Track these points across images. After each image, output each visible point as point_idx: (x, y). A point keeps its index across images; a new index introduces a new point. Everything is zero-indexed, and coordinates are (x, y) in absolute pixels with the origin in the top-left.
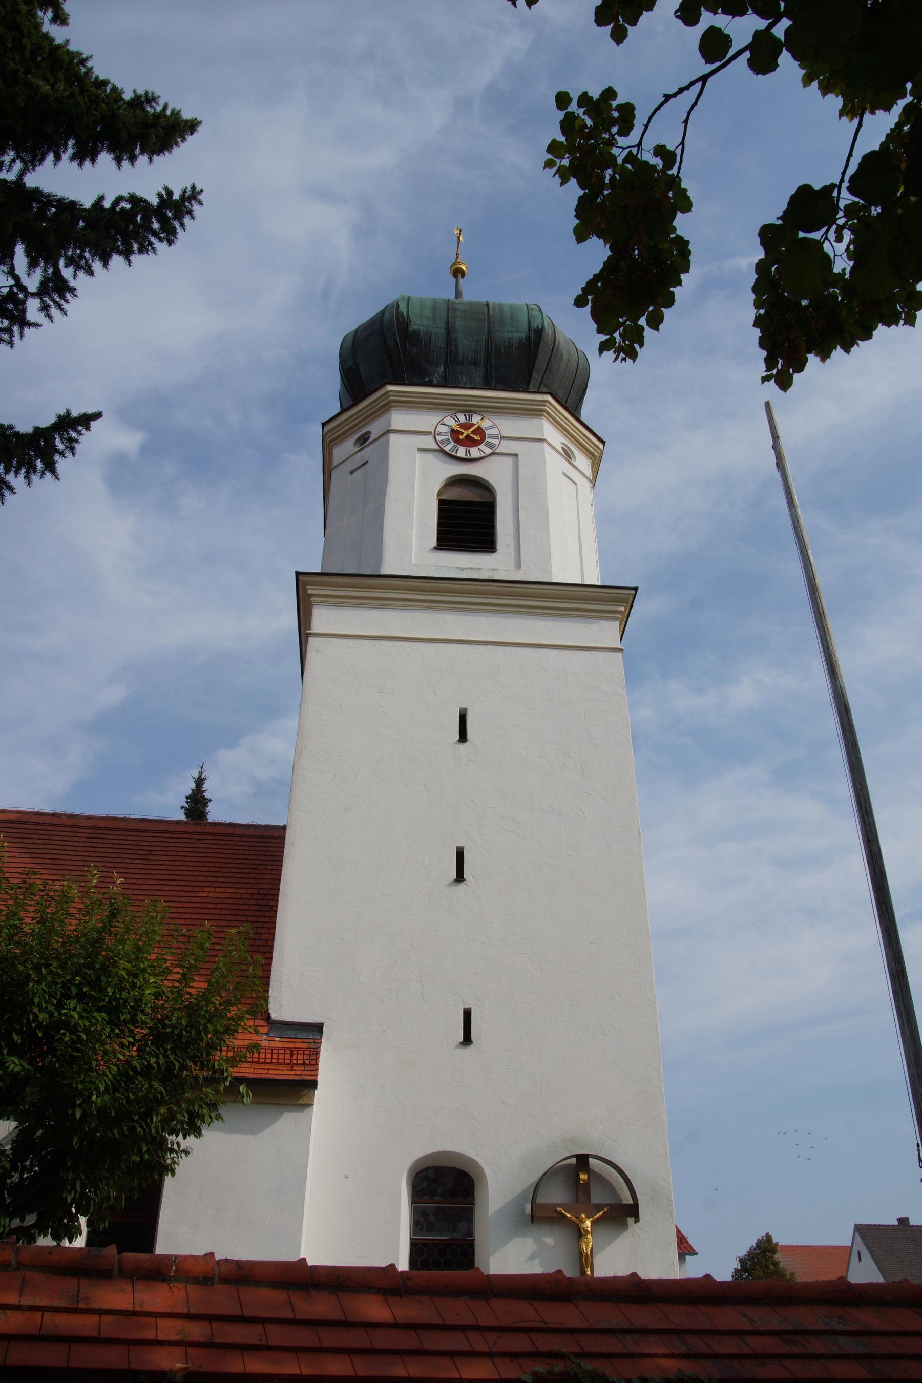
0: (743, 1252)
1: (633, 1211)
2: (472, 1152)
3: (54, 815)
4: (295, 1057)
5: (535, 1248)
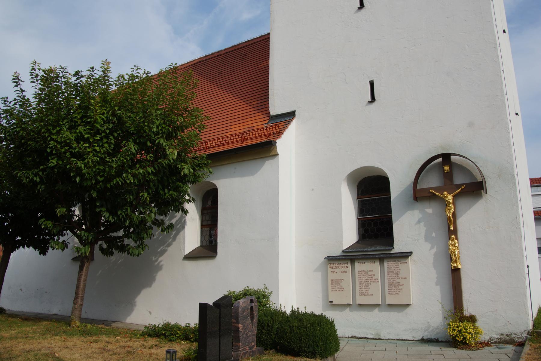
3: (206, 56)
4: (268, 130)
5: (421, 216)
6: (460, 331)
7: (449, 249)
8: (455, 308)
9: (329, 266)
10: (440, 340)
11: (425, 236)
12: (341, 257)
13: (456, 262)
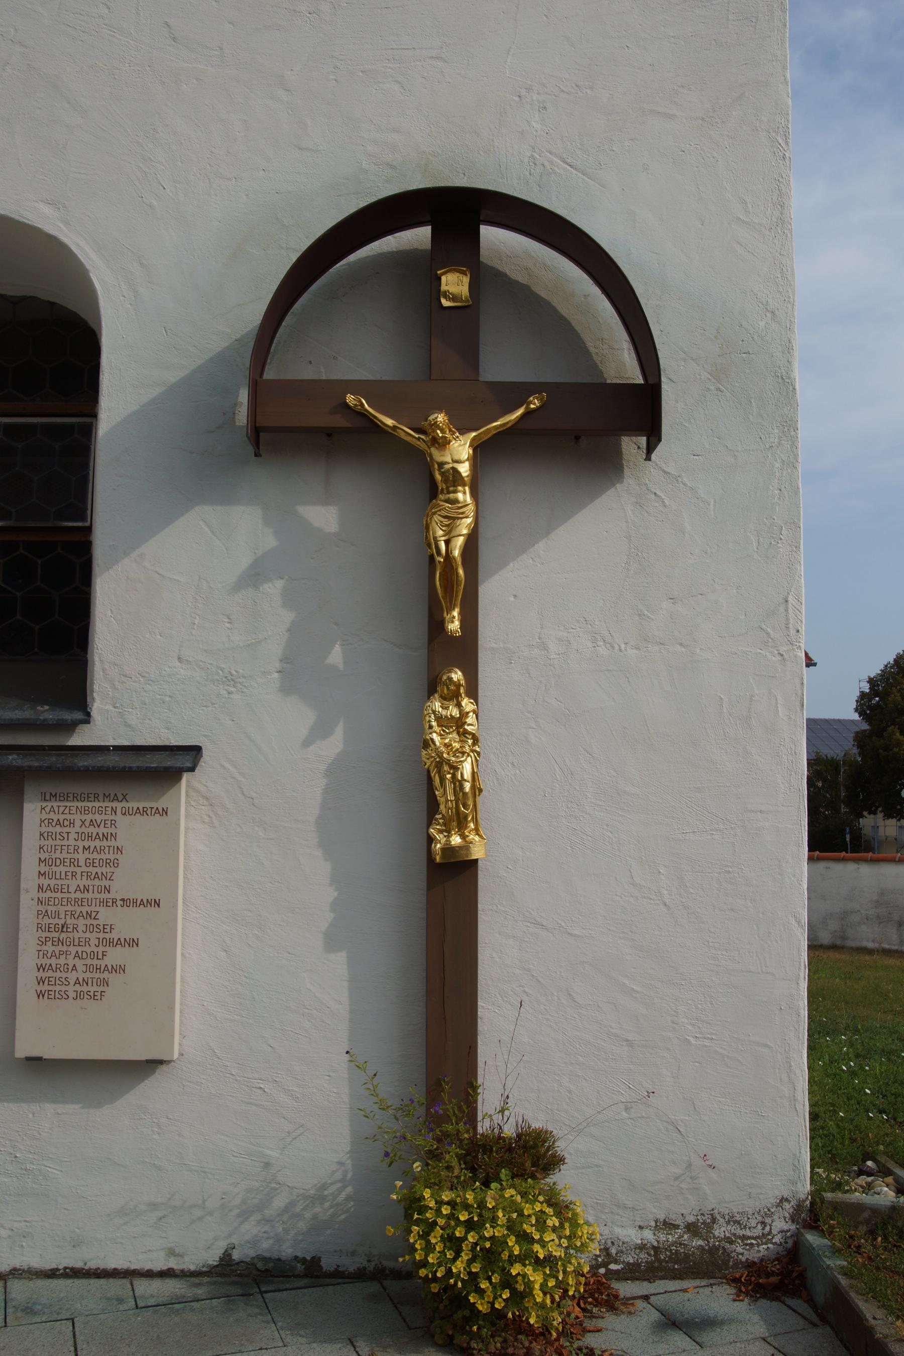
0: (875, 670)
1: (640, 410)
2: (46, 210)
5: (269, 541)
6: (490, 1256)
7: (427, 744)
8: (434, 1089)
10: (328, 1264)
11: (285, 659)
13: (460, 822)
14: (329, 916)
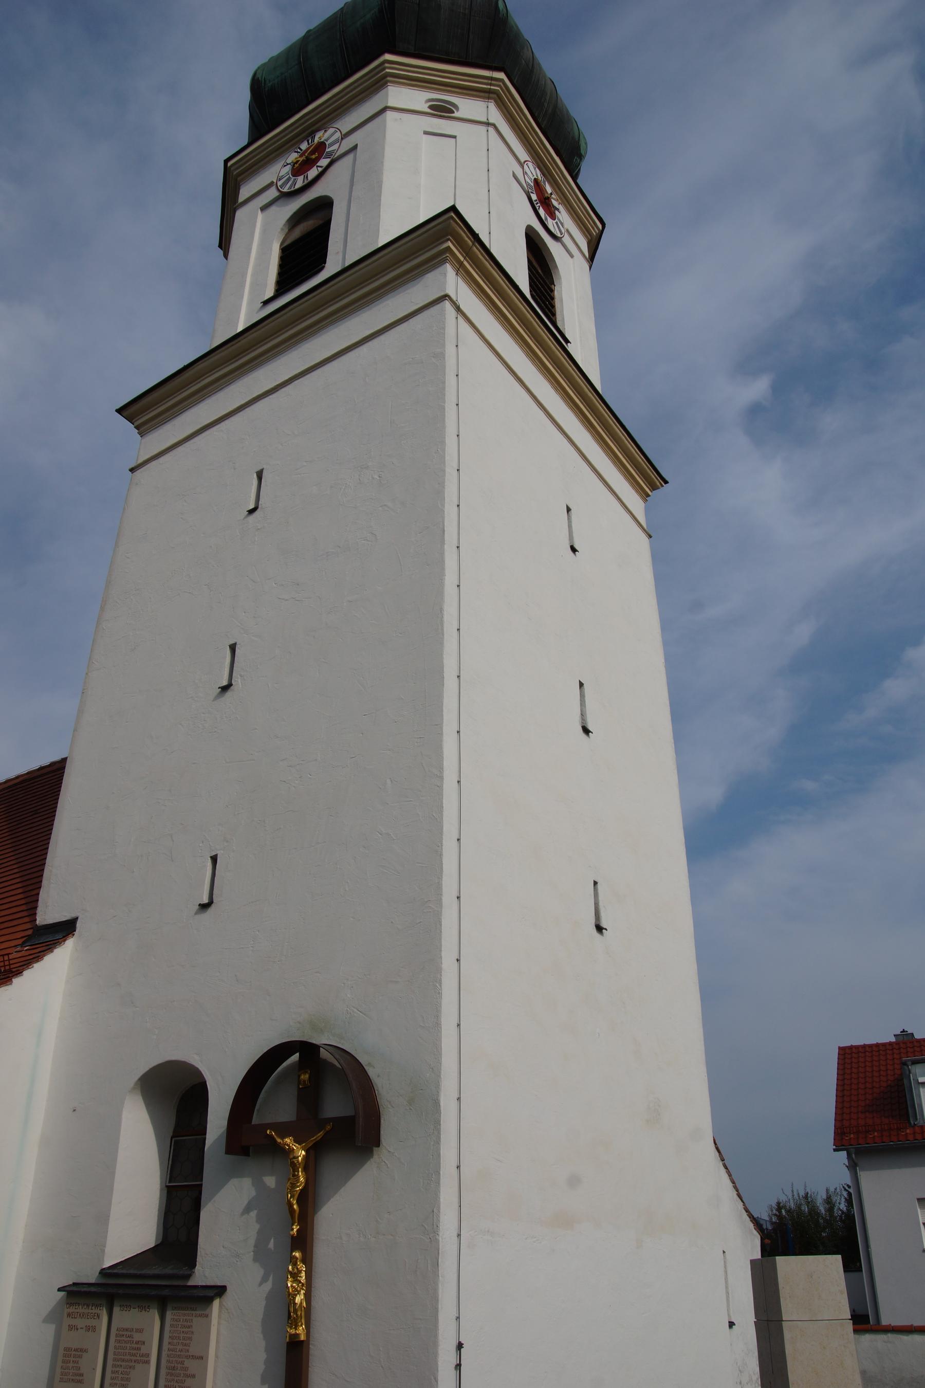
9: (66, 1311)
11: (256, 1246)
12: (93, 1289)
14: (263, 1367)
